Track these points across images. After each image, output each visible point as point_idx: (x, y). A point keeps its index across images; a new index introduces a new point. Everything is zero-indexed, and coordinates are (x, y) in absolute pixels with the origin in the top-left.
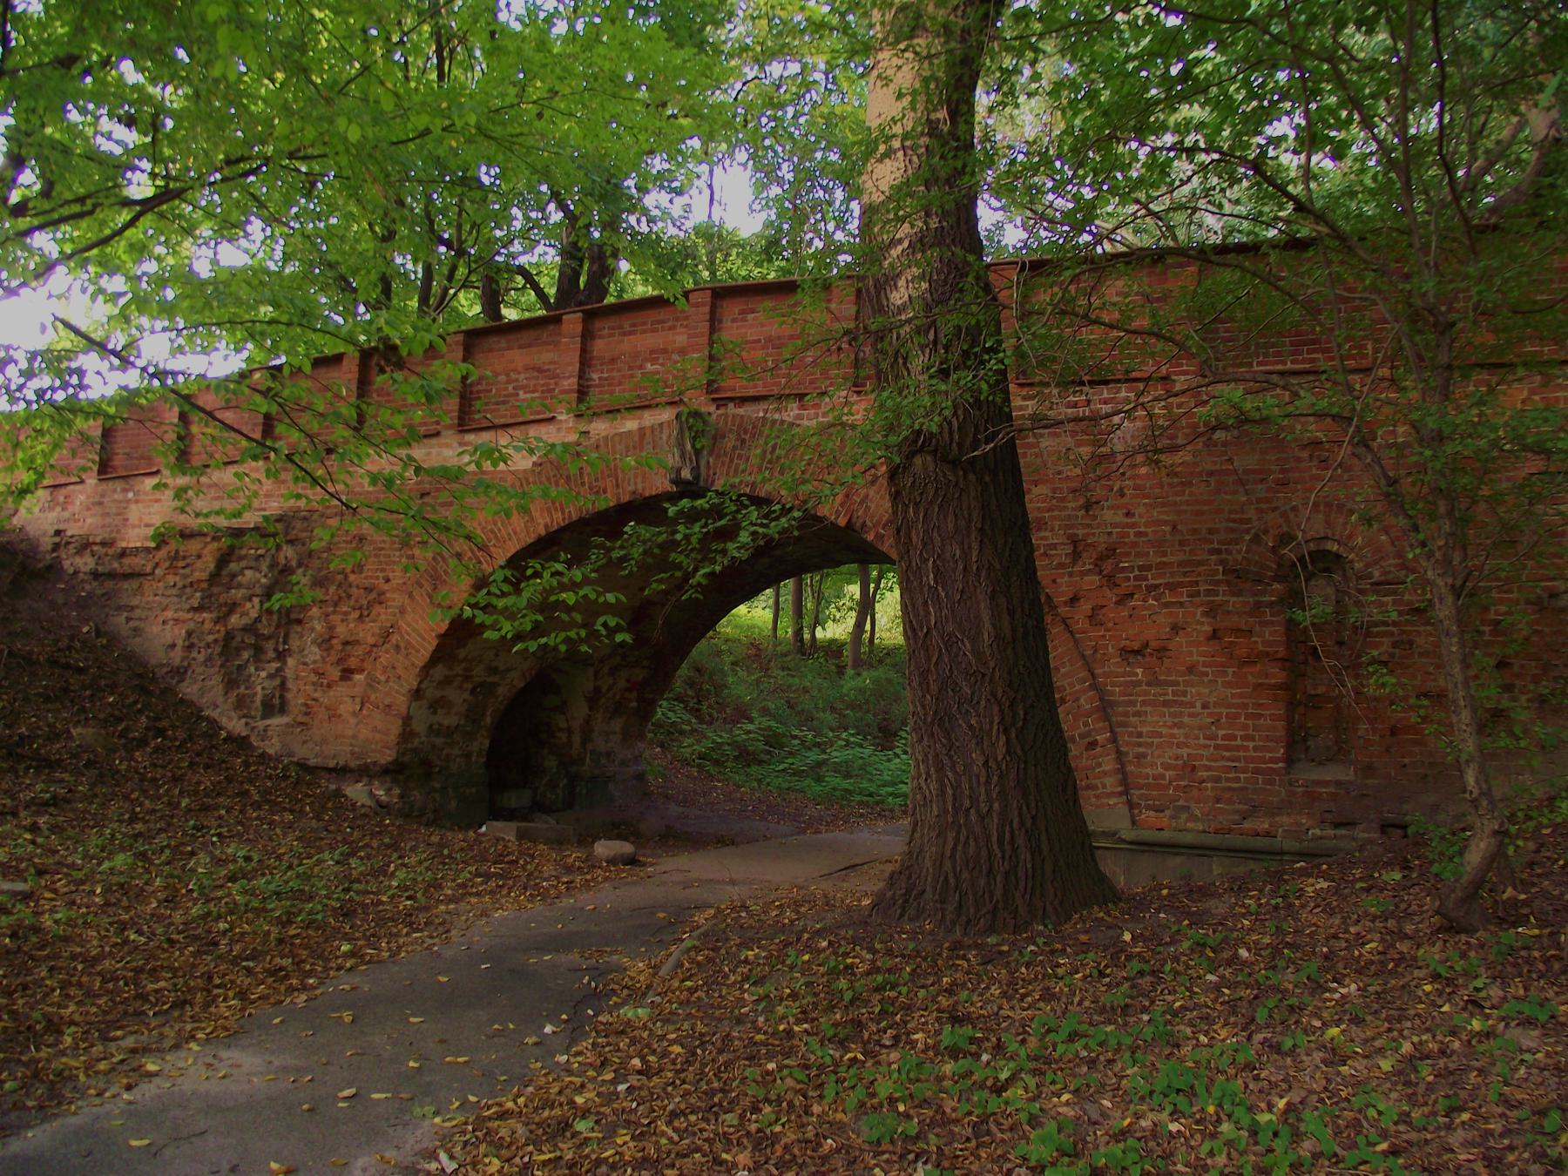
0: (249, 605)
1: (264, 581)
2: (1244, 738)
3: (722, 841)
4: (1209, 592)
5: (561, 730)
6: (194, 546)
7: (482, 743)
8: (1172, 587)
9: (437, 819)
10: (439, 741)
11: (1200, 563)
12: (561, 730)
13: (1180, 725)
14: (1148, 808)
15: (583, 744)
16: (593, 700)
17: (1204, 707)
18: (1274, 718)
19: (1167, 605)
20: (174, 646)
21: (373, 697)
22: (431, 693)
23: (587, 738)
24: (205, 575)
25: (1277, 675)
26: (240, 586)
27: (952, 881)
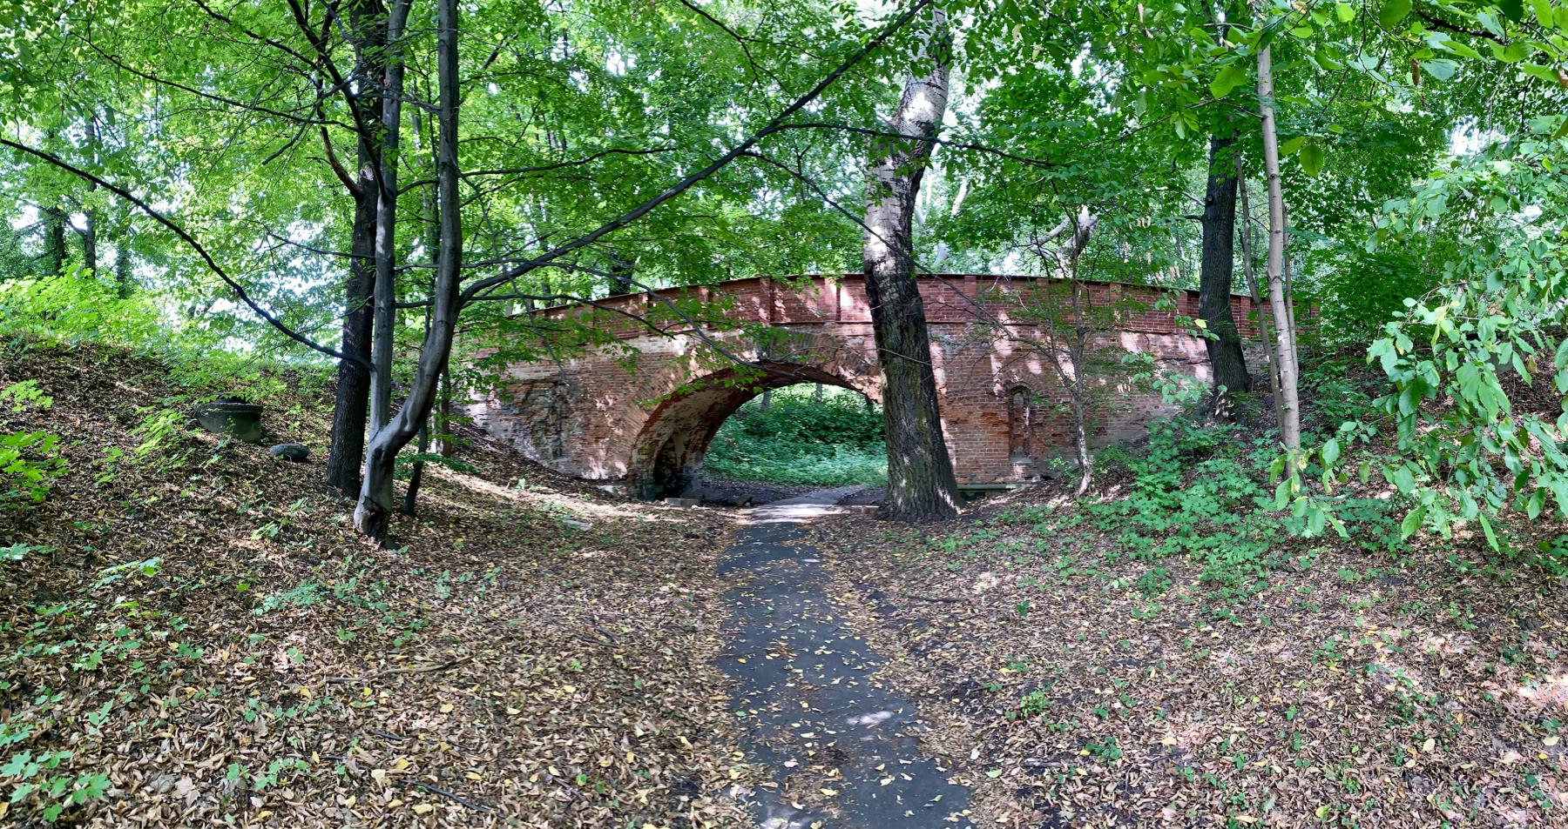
6: (512, 388)
9: (641, 497)
16: (687, 446)
23: (683, 461)
25: (1006, 429)
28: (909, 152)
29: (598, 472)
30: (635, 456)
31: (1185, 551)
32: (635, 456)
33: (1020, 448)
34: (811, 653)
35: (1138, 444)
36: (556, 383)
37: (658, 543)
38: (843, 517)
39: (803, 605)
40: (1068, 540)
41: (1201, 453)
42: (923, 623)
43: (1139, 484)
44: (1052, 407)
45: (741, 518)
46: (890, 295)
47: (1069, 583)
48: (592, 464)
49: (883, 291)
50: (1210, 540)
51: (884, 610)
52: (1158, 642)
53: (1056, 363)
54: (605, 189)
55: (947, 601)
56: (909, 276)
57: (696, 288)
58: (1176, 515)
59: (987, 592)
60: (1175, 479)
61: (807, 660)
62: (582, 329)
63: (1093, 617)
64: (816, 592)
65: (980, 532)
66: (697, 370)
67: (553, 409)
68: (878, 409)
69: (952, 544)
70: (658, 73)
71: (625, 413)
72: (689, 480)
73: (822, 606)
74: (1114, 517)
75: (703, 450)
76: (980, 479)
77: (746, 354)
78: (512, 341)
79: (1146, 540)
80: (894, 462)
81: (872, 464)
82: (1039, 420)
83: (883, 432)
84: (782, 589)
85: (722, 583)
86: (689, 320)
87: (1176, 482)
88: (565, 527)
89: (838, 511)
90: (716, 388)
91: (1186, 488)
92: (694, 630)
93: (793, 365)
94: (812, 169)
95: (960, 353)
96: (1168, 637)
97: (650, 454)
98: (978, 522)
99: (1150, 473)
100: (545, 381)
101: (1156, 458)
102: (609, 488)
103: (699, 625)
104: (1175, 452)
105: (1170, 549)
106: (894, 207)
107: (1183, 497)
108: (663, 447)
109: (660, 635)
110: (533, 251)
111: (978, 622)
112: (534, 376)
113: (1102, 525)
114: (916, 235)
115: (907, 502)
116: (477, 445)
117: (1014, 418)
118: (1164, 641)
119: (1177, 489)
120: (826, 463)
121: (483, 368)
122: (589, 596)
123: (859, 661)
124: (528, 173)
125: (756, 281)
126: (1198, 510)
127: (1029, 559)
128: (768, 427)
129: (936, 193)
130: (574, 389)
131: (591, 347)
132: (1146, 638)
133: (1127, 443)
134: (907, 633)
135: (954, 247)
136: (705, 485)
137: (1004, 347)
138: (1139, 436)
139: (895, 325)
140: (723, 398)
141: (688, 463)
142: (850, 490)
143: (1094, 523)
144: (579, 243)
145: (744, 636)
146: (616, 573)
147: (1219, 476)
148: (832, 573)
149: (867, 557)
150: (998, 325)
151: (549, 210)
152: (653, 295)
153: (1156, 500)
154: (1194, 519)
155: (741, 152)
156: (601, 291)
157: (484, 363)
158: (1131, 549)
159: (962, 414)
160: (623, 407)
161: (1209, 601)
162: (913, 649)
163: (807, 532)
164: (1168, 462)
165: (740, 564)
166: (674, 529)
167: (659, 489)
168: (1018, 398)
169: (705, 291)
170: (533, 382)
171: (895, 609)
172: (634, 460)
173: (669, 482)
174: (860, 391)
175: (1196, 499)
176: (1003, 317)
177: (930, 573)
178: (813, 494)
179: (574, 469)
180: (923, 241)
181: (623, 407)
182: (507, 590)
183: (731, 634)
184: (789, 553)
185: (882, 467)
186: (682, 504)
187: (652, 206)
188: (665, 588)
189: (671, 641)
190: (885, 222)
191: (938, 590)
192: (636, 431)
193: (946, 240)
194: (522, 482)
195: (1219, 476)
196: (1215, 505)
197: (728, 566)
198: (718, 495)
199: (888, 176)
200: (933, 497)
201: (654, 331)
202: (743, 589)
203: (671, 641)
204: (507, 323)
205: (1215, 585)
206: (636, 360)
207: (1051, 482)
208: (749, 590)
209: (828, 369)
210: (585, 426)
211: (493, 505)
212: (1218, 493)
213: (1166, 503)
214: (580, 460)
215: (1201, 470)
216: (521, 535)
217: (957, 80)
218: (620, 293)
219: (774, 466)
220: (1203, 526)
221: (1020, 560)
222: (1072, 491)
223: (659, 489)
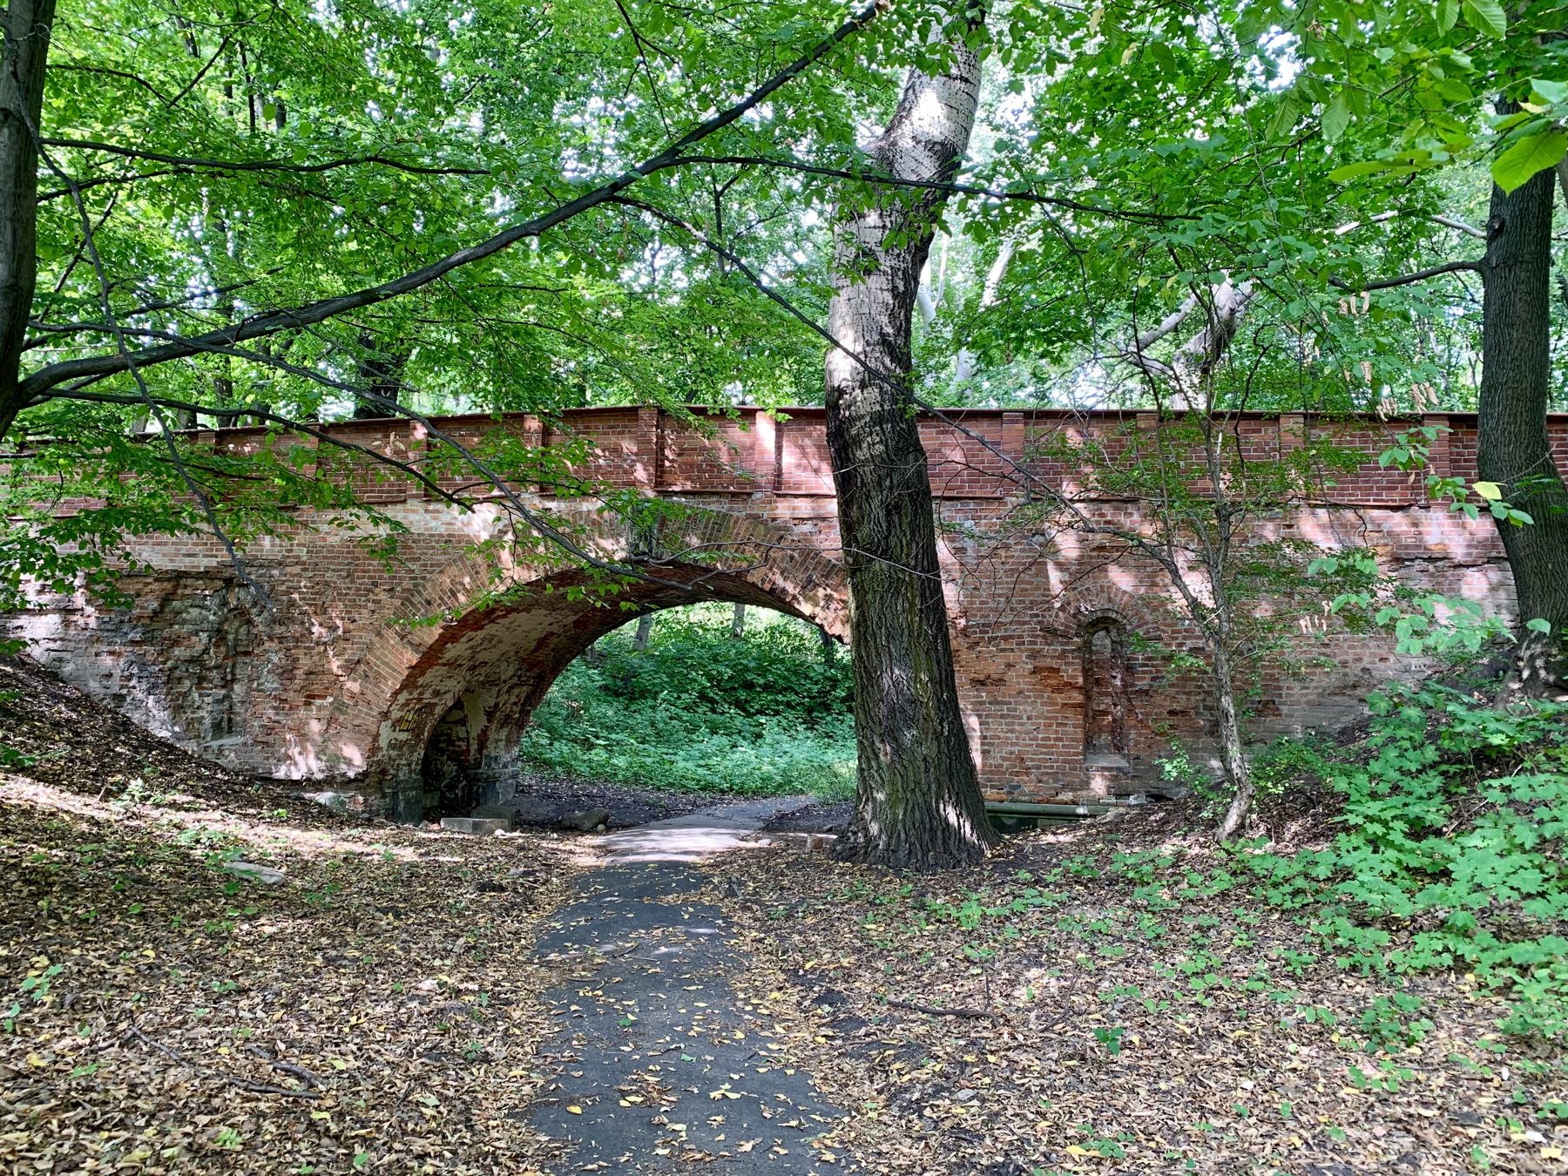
0: (194, 639)
1: (212, 618)
2: (1056, 739)
3: (625, 827)
4: (1031, 643)
5: (459, 739)
6: (132, 587)
7: (420, 753)
8: (1005, 638)
9: (393, 815)
10: (393, 753)
11: (1025, 623)
12: (459, 739)
13: (1012, 731)
14: (992, 787)
15: (480, 751)
16: (490, 715)
17: (1029, 718)
18: (1075, 726)
19: (1002, 650)
20: (110, 675)
21: (341, 719)
22: (396, 714)
23: (482, 745)
24: (148, 612)
25: (1078, 698)
26: (184, 622)
27: (903, 836)
28: (912, 203)
29: (303, 764)
30: (386, 734)
31: (1461, 965)
32: (386, 734)
33: (1105, 738)
34: (703, 1095)
35: (1347, 735)
36: (229, 583)
37: (422, 902)
38: (772, 853)
39: (692, 1012)
40: (1204, 920)
41: (1490, 760)
42: (914, 1051)
43: (1353, 820)
44: (1168, 659)
45: (583, 853)
46: (870, 448)
47: (1209, 1003)
48: (294, 751)
49: (857, 442)
50: (1523, 951)
51: (844, 1025)
52: (1408, 1142)
53: (1175, 573)
54: (359, 219)
55: (964, 1015)
56: (904, 420)
57: (520, 417)
58: (1439, 888)
59: (1042, 1004)
60: (1434, 815)
61: (694, 1105)
62: (289, 479)
63: (1263, 1074)
64: (718, 988)
65: (1028, 892)
66: (517, 573)
67: (219, 635)
68: (843, 653)
69: (974, 911)
70: (467, 17)
71: (370, 647)
72: (491, 781)
73: (727, 1013)
74: (1300, 883)
75: (521, 724)
76: (1030, 793)
77: (608, 544)
78: (137, 488)
79: (1370, 933)
80: (867, 754)
81: (830, 756)
82: (1143, 684)
83: (850, 697)
84: (656, 982)
85: (543, 972)
86: (506, 482)
87: (1434, 818)
88: (228, 876)
89: (764, 843)
90: (553, 605)
91: (1459, 831)
92: (486, 1058)
93: (695, 568)
94: (741, 217)
95: (993, 553)
96: (1430, 1134)
97: (416, 731)
98: (1024, 875)
99: (1374, 796)
100: (207, 575)
101: (1387, 765)
102: (324, 797)
103: (498, 1051)
104: (1431, 753)
105: (1426, 959)
106: (877, 289)
107: (1454, 851)
108: (443, 719)
109: (413, 1071)
110: (204, 313)
111: (1023, 1059)
112: (183, 564)
113: (1275, 897)
114: (918, 339)
115: (890, 829)
116: (31, 705)
117: (1093, 680)
118: (1421, 1142)
119: (1439, 833)
120: (746, 751)
121: (62, 539)
122: (268, 1006)
123: (792, 1111)
124: (193, 163)
125: (631, 413)
126: (1488, 880)
127: (1123, 950)
128: (645, 680)
129: (954, 268)
130: (266, 596)
131: (307, 512)
132: (1380, 1131)
133: (1322, 735)
134: (884, 1068)
135: (986, 358)
136: (521, 790)
137: (1069, 545)
138: (1348, 720)
139: (876, 502)
140: (571, 618)
141: (491, 749)
142: (788, 804)
143: (1259, 891)
144: (299, 318)
145: (580, 1065)
146: (329, 961)
147: (1541, 812)
148: (747, 955)
149: (814, 928)
150: (1057, 502)
151: (241, 235)
152: (437, 423)
153: (1391, 854)
154: (1482, 900)
155: (613, 193)
156: (339, 408)
157: (68, 528)
158: (1340, 950)
159: (994, 667)
160: (367, 637)
161: (1529, 1080)
162: (893, 1095)
163: (705, 879)
164: (1414, 775)
165: (580, 937)
166: (455, 878)
167: (429, 801)
168: (1102, 641)
169: (533, 424)
170: (178, 577)
171: (863, 1023)
172: (383, 742)
173: (452, 787)
174: (810, 619)
175: (1484, 857)
176: (1069, 489)
177: (932, 962)
178: (720, 810)
179: (257, 758)
180: (931, 352)
181: (367, 637)
182: (75, 1009)
183: (555, 1062)
184: (670, 916)
185: (846, 763)
186: (476, 827)
187: (453, 274)
188: (427, 984)
189: (436, 1080)
190: (863, 324)
191: (944, 994)
192: (393, 684)
193: (972, 346)
194: (136, 785)
195: (1541, 812)
196: (1536, 876)
197: (556, 942)
198: (546, 810)
199: (872, 238)
200: (935, 822)
201: (432, 492)
202: (583, 982)
203: (436, 1080)
204: (127, 454)
205: (1541, 1050)
206: (396, 547)
207: (1169, 808)
208: (593, 984)
209: (754, 578)
210: (287, 673)
211: (60, 836)
212: (1539, 849)
213: (1414, 863)
214: (268, 741)
215: (1495, 796)
216: (121, 896)
217: (995, 69)
218: (379, 416)
219: (652, 755)
220: (1505, 917)
221: (1104, 949)
222: (1213, 824)
223: (429, 801)
